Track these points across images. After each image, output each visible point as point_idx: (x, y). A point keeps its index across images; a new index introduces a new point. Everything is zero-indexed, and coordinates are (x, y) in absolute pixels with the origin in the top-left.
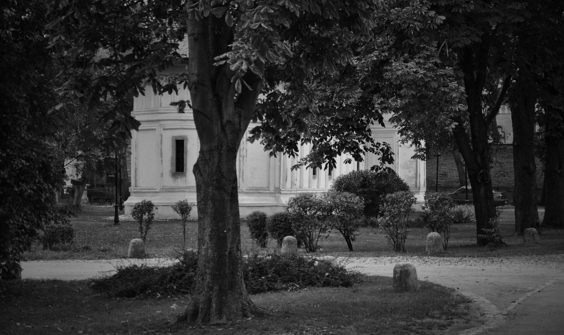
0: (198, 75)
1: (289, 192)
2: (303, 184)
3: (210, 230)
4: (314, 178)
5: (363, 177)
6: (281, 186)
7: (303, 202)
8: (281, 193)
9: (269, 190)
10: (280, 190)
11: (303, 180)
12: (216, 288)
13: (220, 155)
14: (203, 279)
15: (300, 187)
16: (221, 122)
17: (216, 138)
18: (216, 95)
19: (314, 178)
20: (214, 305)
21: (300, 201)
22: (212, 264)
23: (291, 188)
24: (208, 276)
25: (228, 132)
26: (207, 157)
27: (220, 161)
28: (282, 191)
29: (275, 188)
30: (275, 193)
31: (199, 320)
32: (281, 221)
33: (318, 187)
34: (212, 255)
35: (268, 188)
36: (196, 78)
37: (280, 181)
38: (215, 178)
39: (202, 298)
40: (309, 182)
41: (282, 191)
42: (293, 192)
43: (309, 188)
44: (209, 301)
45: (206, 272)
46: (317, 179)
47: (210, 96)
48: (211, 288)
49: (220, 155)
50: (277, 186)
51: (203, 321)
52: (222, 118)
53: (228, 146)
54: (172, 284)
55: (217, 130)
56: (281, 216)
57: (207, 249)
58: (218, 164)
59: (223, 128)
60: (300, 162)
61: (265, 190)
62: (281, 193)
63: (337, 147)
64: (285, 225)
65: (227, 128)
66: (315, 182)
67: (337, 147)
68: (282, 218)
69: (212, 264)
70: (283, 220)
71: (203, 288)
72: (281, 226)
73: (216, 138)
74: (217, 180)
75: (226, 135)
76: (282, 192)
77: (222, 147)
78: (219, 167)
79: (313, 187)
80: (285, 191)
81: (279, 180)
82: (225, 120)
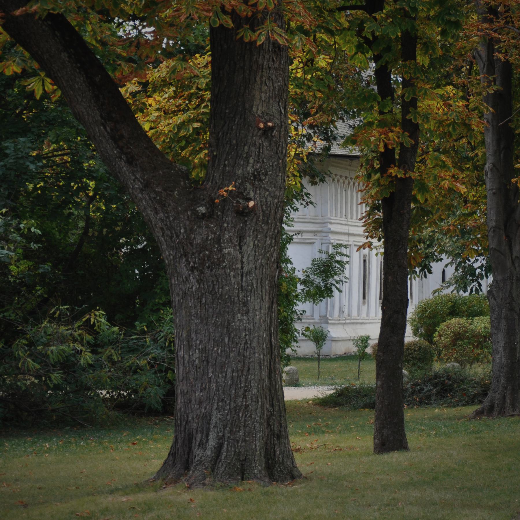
0: (496, 221)
1: (337, 322)
2: (352, 311)
3: (504, 342)
4: (364, 303)
5: (451, 302)
6: (328, 313)
7: (456, 328)
8: (328, 323)
9: (314, 319)
10: (328, 319)
11: (352, 307)
12: (509, 387)
13: (512, 283)
14: (498, 381)
15: (349, 315)
16: (512, 258)
17: (509, 270)
18: (507, 236)
19: (364, 303)
20: (508, 401)
21: (454, 327)
22: (505, 369)
23: (339, 316)
24: (502, 379)
25: (517, 265)
26: (501, 285)
27: (511, 288)
28: (330, 320)
29: (320, 317)
30: (321, 323)
31: (495, 412)
32: (415, 351)
33: (367, 316)
34: (506, 362)
35: (312, 316)
36: (494, 223)
37: (327, 308)
38: (508, 301)
39: (497, 396)
40: (359, 309)
41: (330, 320)
42: (341, 322)
43: (358, 316)
44: (504, 397)
45: (500, 376)
46: (366, 305)
47: (504, 237)
48: (506, 388)
49: (512, 283)
50: (323, 314)
51: (499, 413)
52: (512, 254)
53: (517, 276)
54: (415, 397)
55: (509, 263)
56: (414, 344)
57: (501, 357)
58: (510, 290)
59: (513, 262)
60: (442, 286)
61: (309, 319)
62: (328, 323)
63: (484, 269)
64: (419, 354)
65: (516, 263)
66: (364, 308)
67: (484, 269)
68: (415, 347)
69: (505, 369)
70: (416, 349)
71: (499, 388)
72: (414, 356)
73: (509, 270)
74: (509, 303)
75: (515, 268)
76: (330, 322)
77: (513, 277)
78: (510, 293)
79: (362, 316)
80: (332, 320)
81: (325, 306)
82: (514, 256)
